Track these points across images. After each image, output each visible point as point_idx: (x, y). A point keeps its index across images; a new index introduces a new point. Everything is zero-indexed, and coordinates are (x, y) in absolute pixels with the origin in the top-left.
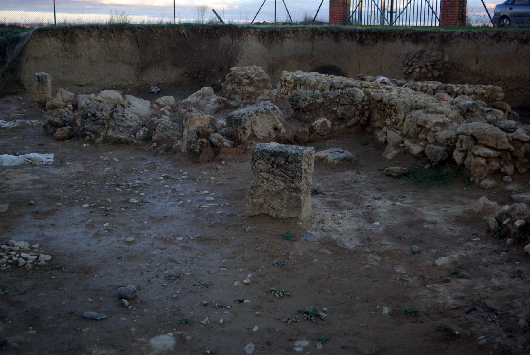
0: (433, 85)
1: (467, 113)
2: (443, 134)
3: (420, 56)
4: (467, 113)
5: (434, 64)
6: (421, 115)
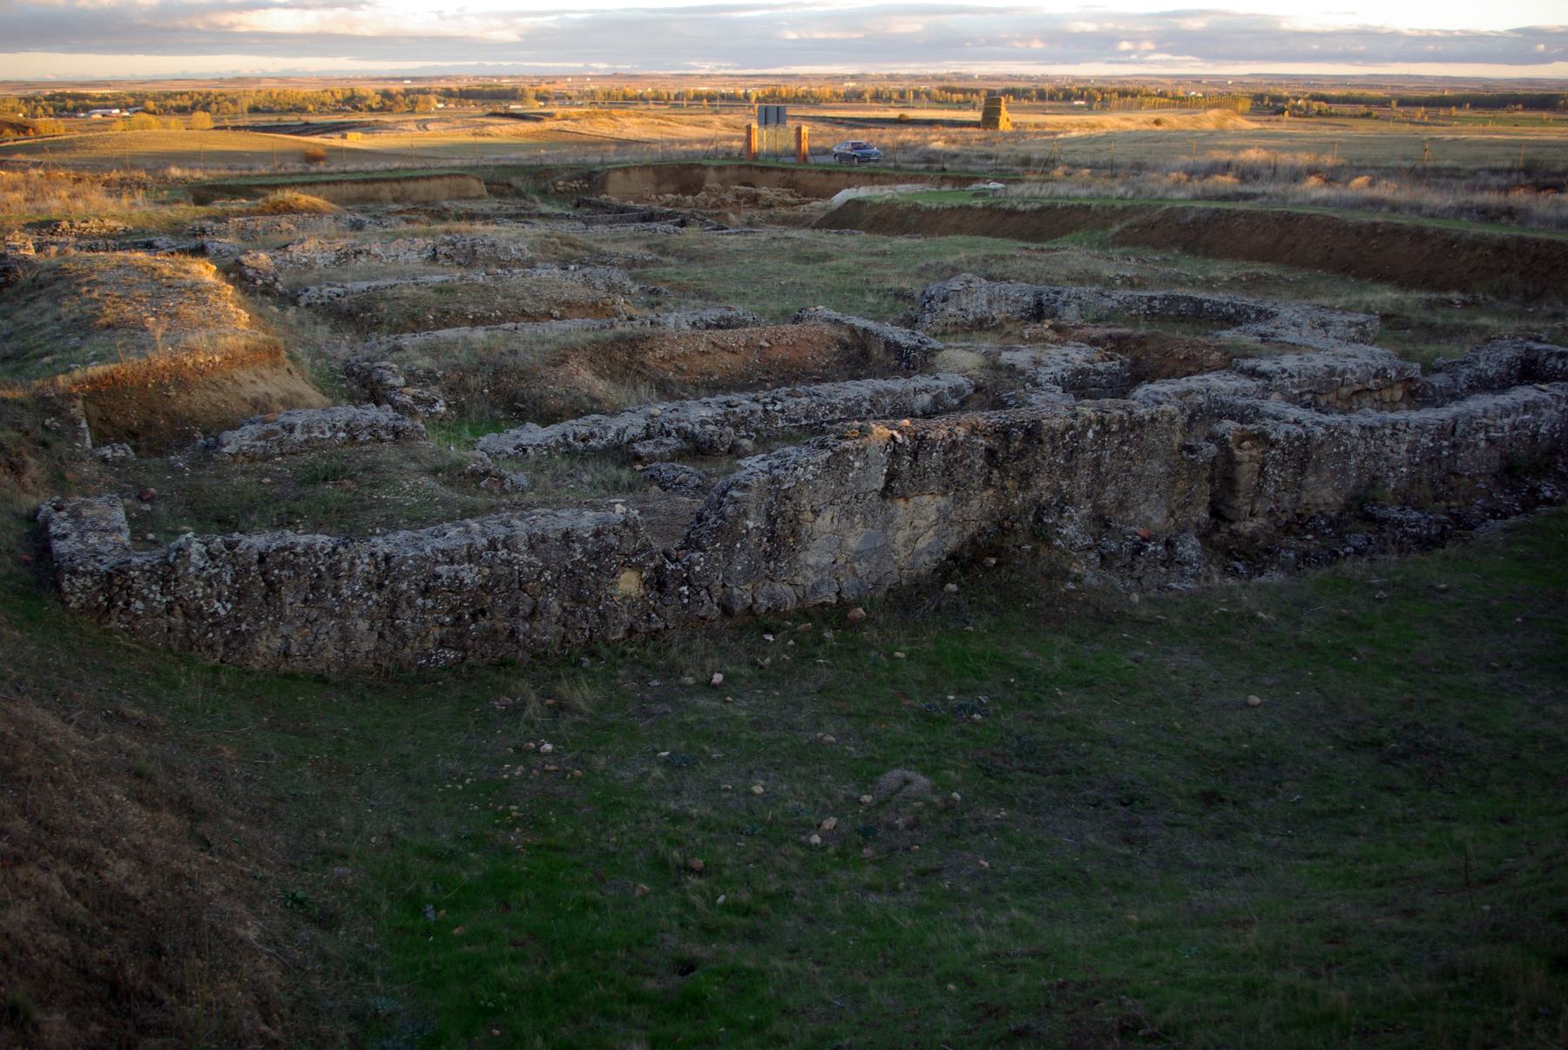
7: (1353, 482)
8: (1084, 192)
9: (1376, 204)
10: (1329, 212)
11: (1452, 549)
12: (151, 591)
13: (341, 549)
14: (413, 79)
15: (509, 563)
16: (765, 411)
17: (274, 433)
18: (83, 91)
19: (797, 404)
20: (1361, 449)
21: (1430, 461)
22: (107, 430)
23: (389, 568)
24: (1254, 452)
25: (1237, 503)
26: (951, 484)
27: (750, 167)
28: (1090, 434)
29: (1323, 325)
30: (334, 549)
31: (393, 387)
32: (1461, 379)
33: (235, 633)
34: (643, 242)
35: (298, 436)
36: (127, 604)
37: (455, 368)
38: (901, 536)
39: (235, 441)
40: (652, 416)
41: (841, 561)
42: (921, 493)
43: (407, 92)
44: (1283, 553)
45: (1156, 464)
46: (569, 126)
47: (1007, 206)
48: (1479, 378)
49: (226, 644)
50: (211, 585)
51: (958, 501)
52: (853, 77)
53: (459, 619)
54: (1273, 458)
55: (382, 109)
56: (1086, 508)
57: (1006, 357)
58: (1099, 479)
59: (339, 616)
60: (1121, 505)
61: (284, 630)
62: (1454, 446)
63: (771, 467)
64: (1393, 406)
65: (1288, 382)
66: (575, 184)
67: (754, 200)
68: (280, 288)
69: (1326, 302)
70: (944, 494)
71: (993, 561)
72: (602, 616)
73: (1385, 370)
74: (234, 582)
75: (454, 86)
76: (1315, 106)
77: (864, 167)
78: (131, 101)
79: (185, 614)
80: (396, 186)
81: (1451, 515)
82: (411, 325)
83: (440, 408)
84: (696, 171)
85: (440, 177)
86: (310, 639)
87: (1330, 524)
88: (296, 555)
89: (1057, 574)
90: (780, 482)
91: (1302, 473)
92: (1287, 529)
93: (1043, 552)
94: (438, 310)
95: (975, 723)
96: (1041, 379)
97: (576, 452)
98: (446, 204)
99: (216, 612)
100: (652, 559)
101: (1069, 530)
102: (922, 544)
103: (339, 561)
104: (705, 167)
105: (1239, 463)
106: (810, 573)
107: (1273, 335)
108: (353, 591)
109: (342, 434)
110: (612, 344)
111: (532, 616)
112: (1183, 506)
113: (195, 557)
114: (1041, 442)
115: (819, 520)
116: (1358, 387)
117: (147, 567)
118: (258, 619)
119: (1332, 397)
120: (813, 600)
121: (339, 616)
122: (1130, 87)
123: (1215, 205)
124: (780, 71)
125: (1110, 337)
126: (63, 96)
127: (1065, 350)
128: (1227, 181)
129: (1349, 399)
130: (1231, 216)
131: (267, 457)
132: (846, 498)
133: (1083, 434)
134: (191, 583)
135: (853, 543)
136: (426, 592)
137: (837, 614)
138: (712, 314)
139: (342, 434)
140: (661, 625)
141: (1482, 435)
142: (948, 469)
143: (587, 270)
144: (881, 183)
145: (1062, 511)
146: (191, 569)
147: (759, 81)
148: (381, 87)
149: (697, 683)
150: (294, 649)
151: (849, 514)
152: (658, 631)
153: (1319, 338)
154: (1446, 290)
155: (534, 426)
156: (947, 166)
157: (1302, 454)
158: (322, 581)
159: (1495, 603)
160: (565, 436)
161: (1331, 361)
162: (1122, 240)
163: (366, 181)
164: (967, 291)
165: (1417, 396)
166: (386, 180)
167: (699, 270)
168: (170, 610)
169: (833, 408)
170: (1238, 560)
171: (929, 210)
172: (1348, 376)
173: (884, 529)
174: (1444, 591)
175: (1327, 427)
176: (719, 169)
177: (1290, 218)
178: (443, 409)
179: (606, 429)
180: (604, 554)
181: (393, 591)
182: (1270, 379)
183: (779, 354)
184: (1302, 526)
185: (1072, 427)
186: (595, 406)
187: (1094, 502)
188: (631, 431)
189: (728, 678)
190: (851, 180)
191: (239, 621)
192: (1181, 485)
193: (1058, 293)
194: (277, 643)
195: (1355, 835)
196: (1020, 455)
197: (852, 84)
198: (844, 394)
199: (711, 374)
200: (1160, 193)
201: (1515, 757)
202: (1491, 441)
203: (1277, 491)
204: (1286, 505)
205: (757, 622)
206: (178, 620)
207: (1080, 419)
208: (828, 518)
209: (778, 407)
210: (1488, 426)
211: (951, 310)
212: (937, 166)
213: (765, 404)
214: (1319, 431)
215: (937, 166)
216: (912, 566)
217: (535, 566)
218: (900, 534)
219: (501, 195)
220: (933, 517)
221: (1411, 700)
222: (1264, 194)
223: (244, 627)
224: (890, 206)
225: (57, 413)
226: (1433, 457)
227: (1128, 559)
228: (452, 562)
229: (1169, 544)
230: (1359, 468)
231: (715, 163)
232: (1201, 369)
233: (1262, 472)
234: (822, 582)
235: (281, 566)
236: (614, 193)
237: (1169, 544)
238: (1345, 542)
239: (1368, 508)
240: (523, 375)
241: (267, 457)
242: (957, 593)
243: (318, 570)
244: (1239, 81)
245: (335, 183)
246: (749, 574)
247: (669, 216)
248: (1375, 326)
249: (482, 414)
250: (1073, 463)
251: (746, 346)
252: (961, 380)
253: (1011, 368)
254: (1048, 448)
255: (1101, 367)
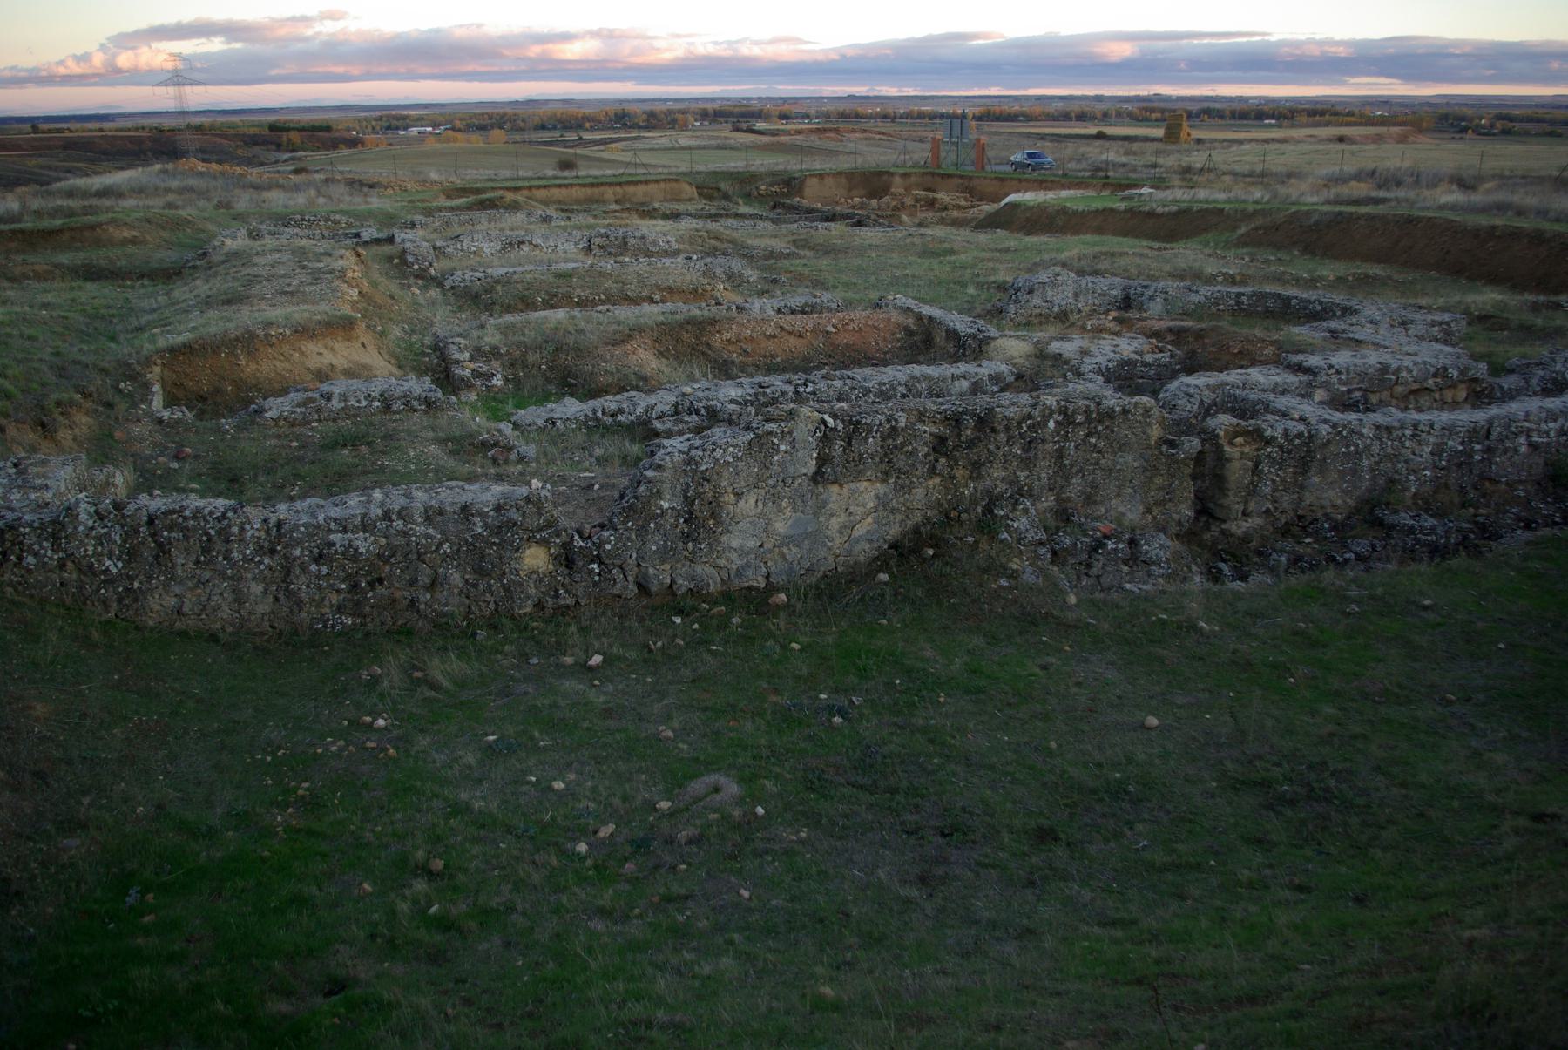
7: (1365, 484)
8: (1222, 196)
9: (1501, 208)
10: (1451, 216)
11: (1460, 561)
12: (42, 547)
13: (230, 514)
15: (405, 533)
16: (797, 392)
17: (313, 400)
19: (829, 387)
20: (1376, 449)
21: (1460, 465)
22: (180, 394)
23: (280, 535)
24: (1246, 449)
25: (1225, 502)
26: (888, 466)
27: (933, 174)
28: (1051, 424)
29: (1404, 323)
30: (224, 514)
31: (457, 362)
32: (1534, 381)
33: (127, 590)
34: (791, 238)
35: (336, 404)
36: (20, 558)
37: (519, 345)
38: (835, 523)
39: (276, 407)
40: (684, 394)
41: (768, 546)
42: (856, 479)
44: (1274, 555)
45: (1129, 458)
47: (1147, 208)
48: (1555, 380)
49: (120, 600)
50: (101, 544)
51: (901, 489)
53: (355, 587)
54: (1269, 455)
55: (648, 128)
56: (1048, 501)
57: (1055, 346)
58: (1063, 471)
59: (232, 578)
60: (1089, 500)
61: (177, 590)
62: (1489, 450)
63: (691, 447)
64: (1455, 405)
65: (1334, 379)
66: (776, 188)
67: (931, 204)
68: (432, 272)
69: (1423, 302)
70: (884, 481)
71: (931, 552)
72: (507, 589)
73: (1445, 369)
74: (125, 542)
76: (1499, 124)
77: (1035, 175)
79: (80, 570)
80: (618, 189)
81: (1476, 523)
82: (520, 306)
83: (498, 381)
85: (657, 181)
86: (203, 599)
87: (1334, 528)
88: (185, 518)
89: (995, 568)
90: (696, 463)
91: (1304, 473)
92: (1285, 532)
93: (984, 546)
94: (547, 293)
95: (832, 727)
96: (1085, 368)
97: (606, 427)
98: (657, 205)
99: (107, 569)
100: (558, 536)
101: (1021, 523)
102: (859, 531)
103: (229, 526)
104: (892, 174)
105: (1229, 460)
106: (734, 556)
107: (1344, 331)
108: (244, 555)
109: (376, 404)
110: (681, 326)
111: (432, 586)
112: (1162, 503)
113: (83, 517)
114: (994, 430)
115: (742, 503)
116: (1416, 386)
117: (36, 525)
118: (150, 578)
119: (1385, 395)
120: (737, 584)
121: (232, 578)
122: (1319, 107)
123: (1338, 209)
125: (1170, 330)
127: (1118, 341)
128: (1360, 189)
129: (1405, 398)
130: (1352, 218)
131: (306, 422)
132: (771, 482)
133: (1044, 424)
134: (81, 541)
135: (781, 527)
136: (318, 559)
137: (756, 601)
138: (797, 301)
139: (376, 404)
140: (570, 601)
141: (1522, 440)
142: (887, 456)
143: (708, 260)
144: (1046, 189)
145: (1017, 503)
146: (81, 528)
149: (576, 664)
150: (186, 609)
151: (775, 498)
152: (568, 607)
153: (1396, 334)
154: (1557, 293)
155: (573, 400)
156: (1111, 174)
157: (1304, 453)
158: (213, 542)
159: (1480, 625)
160: (594, 411)
161: (1387, 358)
162: (1243, 242)
163: (592, 185)
164: (1053, 283)
165: (1480, 395)
166: (610, 184)
167: (825, 262)
168: (62, 565)
169: (867, 392)
170: (1224, 561)
171: (1075, 213)
172: (1404, 374)
173: (816, 515)
174: (1425, 608)
175: (1334, 426)
176: (905, 175)
177: (1410, 220)
178: (500, 383)
179: (635, 405)
180: (507, 529)
181: (285, 557)
182: (1315, 374)
183: (844, 339)
184: (1304, 528)
185: (1030, 416)
186: (645, 383)
187: (1058, 495)
188: (660, 408)
189: (609, 660)
190: (1023, 185)
191: (131, 579)
192: (1158, 481)
193: (1146, 287)
194: (171, 601)
195: (1182, 897)
196: (972, 443)
198: (878, 379)
199: (773, 357)
200: (1294, 198)
201: (1421, 815)
202: (1533, 447)
203: (1275, 490)
204: (1285, 505)
205: (675, 601)
206: (71, 574)
207: (1040, 408)
208: (752, 502)
209: (810, 389)
210: (1529, 430)
211: (1036, 301)
212: (1102, 174)
213: (797, 386)
214: (1324, 429)
215: (1102, 174)
216: (849, 553)
217: (432, 538)
218: (834, 520)
219: (710, 198)
220: (871, 504)
221: (1332, 735)
222: (1397, 199)
223: (136, 585)
224: (1042, 208)
225: (133, 377)
226: (1462, 461)
227: (1085, 556)
228: (345, 530)
229: (1132, 542)
230: (1373, 470)
231: (901, 171)
232: (1254, 363)
233: (1256, 470)
234: (748, 565)
235: (170, 528)
236: (812, 195)
237: (1132, 542)
238: (1347, 547)
239: (1379, 512)
240: (579, 352)
241: (306, 422)
242: (886, 584)
243: (207, 534)
244: (1427, 103)
245: (566, 186)
246: (665, 554)
247: (844, 217)
248: (1460, 326)
249: (535, 388)
250: (1031, 454)
251: (813, 331)
252: (1003, 368)
253: (1057, 357)
254: (1002, 437)
255: (1149, 358)
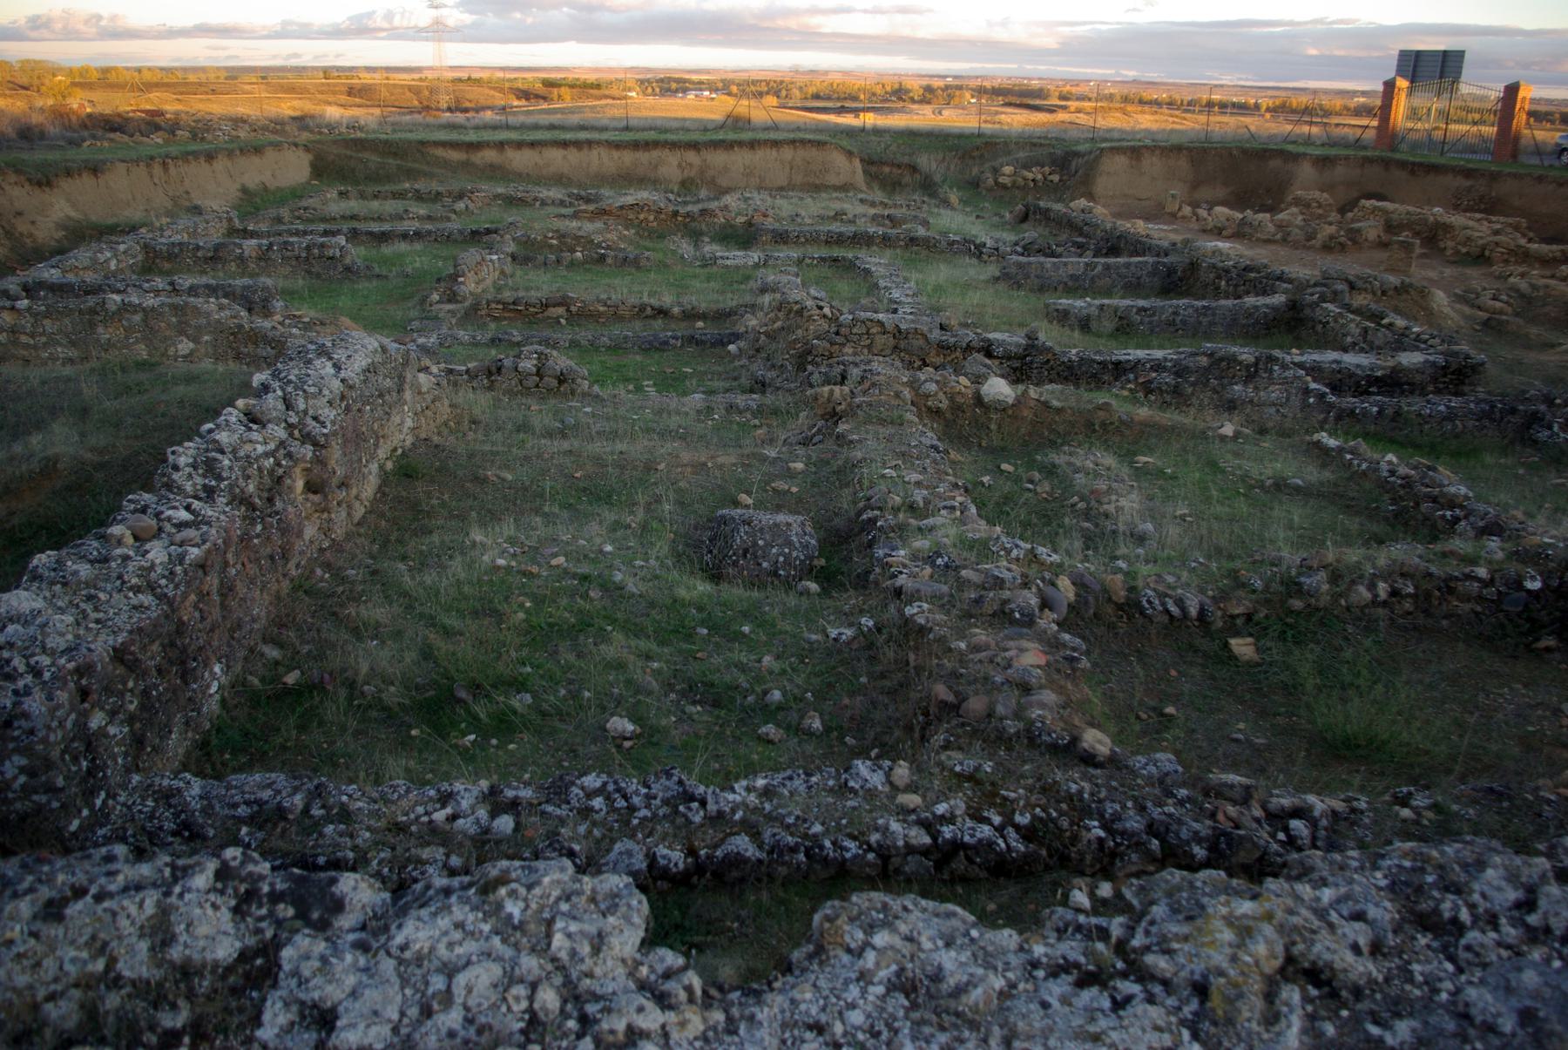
0: (1478, 216)
1: (1497, 233)
2: (1481, 242)
3: (1469, 189)
4: (1497, 233)
5: (1481, 198)
6: (1469, 232)
14: (955, 77)
18: (687, 76)
27: (1387, 163)
43: (947, 87)
46: (1082, 119)
52: (1364, 93)
66: (1035, 174)
75: (987, 84)
78: (720, 85)
80: (691, 156)
84: (1275, 163)
85: (775, 144)
104: (1295, 158)
124: (1291, 85)
126: (670, 80)
147: (1270, 93)
148: (925, 82)
163: (636, 145)
166: (674, 146)
176: (1324, 162)
197: (1362, 100)
219: (892, 186)
245: (578, 144)
